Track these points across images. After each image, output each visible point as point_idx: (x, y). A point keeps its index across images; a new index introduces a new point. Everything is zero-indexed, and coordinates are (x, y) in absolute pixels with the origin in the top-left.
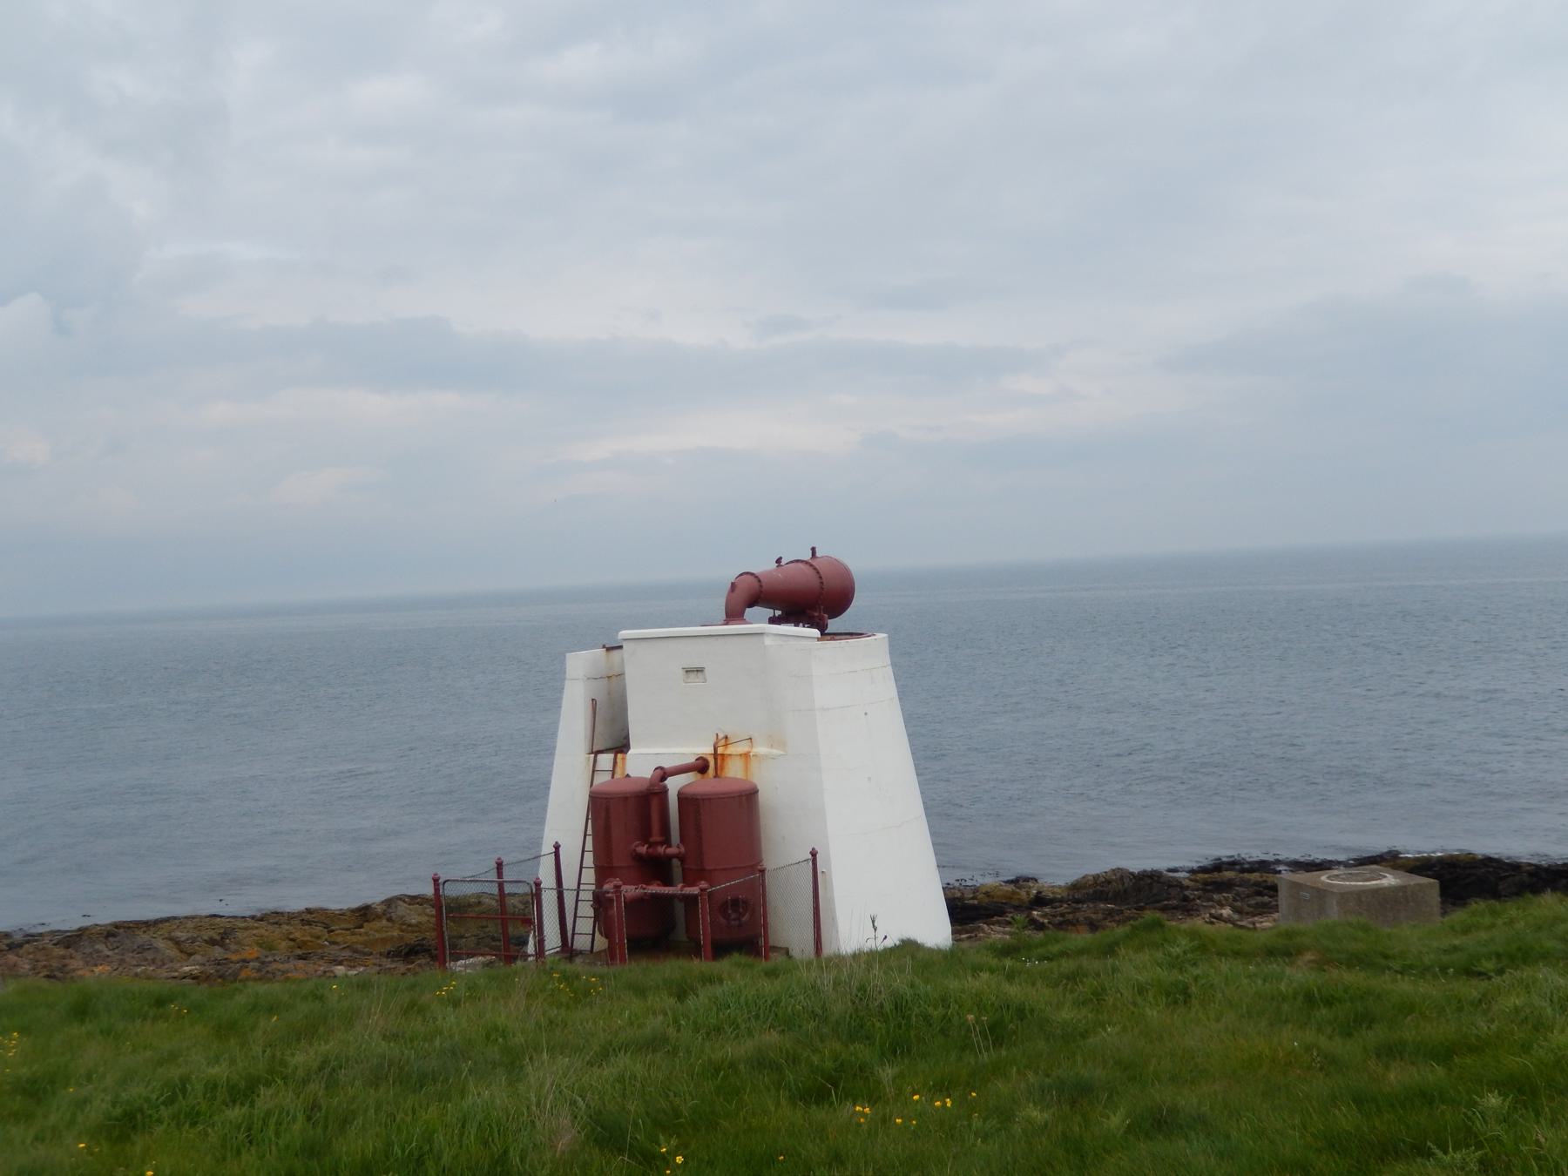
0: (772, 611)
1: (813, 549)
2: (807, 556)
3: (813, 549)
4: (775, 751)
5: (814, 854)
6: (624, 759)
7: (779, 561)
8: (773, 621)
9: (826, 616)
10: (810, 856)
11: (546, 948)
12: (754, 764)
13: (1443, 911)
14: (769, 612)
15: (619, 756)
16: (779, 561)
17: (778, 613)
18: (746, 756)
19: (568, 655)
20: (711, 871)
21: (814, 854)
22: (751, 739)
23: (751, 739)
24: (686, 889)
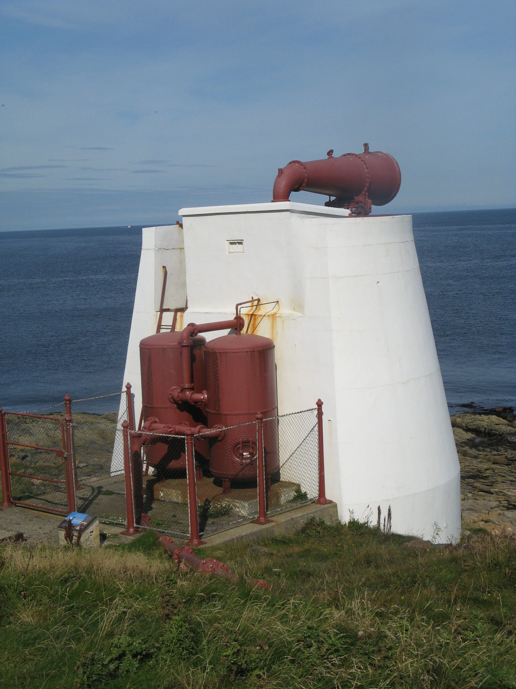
0: (328, 197)
1: (366, 145)
2: (360, 150)
3: (366, 145)
4: (296, 313)
5: (320, 404)
6: (182, 316)
7: (330, 153)
8: (328, 204)
9: (370, 201)
10: (316, 407)
11: (112, 470)
12: (278, 321)
13: (463, 497)
14: (326, 198)
15: (179, 314)
16: (330, 153)
17: (333, 198)
18: (273, 316)
19: (144, 229)
20: (226, 415)
21: (320, 404)
22: (278, 302)
23: (278, 302)
24: (204, 430)
